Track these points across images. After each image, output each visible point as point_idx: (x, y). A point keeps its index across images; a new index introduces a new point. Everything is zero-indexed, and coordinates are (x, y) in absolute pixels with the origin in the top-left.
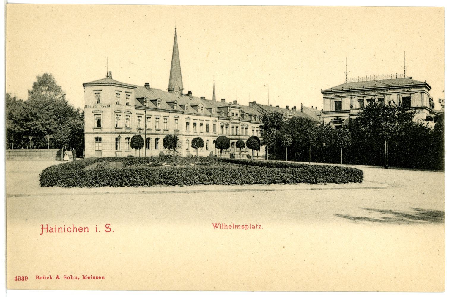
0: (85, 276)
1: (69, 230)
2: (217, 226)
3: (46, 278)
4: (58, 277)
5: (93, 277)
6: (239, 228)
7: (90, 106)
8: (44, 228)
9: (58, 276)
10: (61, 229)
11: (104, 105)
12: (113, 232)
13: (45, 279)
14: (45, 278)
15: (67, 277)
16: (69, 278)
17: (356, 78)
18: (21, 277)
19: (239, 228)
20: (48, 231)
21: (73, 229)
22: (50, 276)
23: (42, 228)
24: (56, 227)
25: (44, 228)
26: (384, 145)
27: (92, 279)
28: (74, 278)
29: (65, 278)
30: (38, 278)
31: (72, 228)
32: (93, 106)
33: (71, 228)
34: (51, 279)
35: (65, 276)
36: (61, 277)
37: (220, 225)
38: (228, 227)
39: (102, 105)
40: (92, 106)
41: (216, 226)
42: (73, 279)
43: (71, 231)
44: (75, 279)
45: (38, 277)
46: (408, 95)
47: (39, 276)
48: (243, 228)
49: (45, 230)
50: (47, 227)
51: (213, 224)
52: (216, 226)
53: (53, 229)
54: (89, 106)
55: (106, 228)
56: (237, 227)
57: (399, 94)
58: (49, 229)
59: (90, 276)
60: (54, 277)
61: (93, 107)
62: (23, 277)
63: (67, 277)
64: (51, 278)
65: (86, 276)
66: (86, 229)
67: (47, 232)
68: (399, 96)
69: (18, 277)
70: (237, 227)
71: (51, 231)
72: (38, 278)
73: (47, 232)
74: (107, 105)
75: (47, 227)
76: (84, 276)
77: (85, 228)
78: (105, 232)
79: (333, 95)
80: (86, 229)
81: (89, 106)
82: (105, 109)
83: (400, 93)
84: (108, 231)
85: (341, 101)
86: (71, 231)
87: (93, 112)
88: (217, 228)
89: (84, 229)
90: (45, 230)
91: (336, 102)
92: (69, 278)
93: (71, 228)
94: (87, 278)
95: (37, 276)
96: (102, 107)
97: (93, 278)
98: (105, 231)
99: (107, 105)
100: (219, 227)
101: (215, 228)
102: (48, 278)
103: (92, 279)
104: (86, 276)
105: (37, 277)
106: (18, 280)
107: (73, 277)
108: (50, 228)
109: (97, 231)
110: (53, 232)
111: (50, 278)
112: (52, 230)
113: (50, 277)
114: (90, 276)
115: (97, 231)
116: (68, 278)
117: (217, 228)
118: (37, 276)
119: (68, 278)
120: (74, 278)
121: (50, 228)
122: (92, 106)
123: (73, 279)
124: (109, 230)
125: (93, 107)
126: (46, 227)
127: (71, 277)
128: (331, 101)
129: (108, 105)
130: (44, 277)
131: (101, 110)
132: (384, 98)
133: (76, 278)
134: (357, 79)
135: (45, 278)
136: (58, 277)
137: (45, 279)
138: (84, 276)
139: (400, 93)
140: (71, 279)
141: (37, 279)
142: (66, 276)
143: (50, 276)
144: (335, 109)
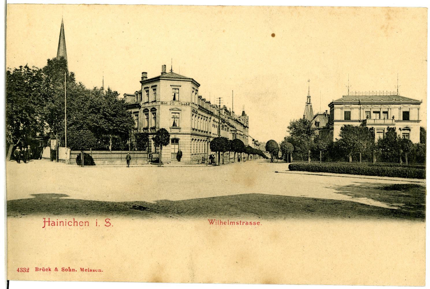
0: (82, 269)
1: (81, 224)
2: (213, 222)
3: (45, 270)
4: (56, 269)
5: (90, 270)
6: (233, 223)
7: (167, 103)
8: (46, 222)
9: (56, 268)
10: (62, 223)
11: (183, 103)
12: (99, 226)
13: (44, 271)
14: (44, 270)
15: (65, 269)
16: (66, 270)
17: (370, 92)
18: (26, 269)
19: (233, 223)
20: (50, 224)
21: (74, 223)
22: (49, 268)
23: (45, 222)
24: (57, 221)
25: (46, 222)
26: (56, 153)
27: (89, 271)
28: (72, 270)
29: (63, 270)
30: (37, 270)
31: (73, 222)
32: (170, 103)
33: (83, 223)
34: (50, 271)
35: (63, 268)
36: (60, 269)
37: (215, 221)
38: (223, 223)
39: (181, 103)
40: (169, 103)
41: (212, 222)
42: (71, 271)
43: (71, 225)
44: (73, 271)
45: (37, 268)
46: (407, 110)
47: (38, 268)
48: (255, 224)
49: (47, 224)
50: (49, 220)
51: (209, 220)
52: (212, 222)
53: (54, 222)
54: (166, 102)
55: (106, 223)
56: (231, 223)
57: (342, 109)
58: (50, 223)
59: (87, 269)
60: (53, 269)
61: (171, 104)
62: (21, 269)
63: (65, 269)
64: (50, 270)
65: (83, 269)
66: (87, 224)
67: (49, 225)
68: (400, 110)
69: (24, 269)
70: (231, 223)
71: (53, 224)
72: (37, 270)
73: (49, 225)
74: (186, 103)
75: (49, 220)
76: (81, 268)
77: (85, 222)
78: (105, 226)
79: (343, 106)
80: (87, 224)
81: (166, 102)
82: (183, 108)
83: (343, 108)
84: (108, 225)
85: (350, 112)
86: (71, 225)
87: (170, 110)
88: (212, 224)
89: (84, 223)
90: (47, 224)
91: (403, 112)
92: (66, 270)
93: (72, 222)
94: (84, 270)
95: (36, 268)
96: (181, 104)
97: (90, 270)
98: (105, 225)
99: (186, 103)
100: (215, 223)
101: (210, 224)
102: (47, 270)
103: (89, 271)
104: (83, 269)
105: (36, 269)
106: (20, 271)
107: (71, 269)
108: (52, 221)
109: (97, 226)
110: (55, 225)
111: (48, 270)
112: (53, 223)
113: (48, 269)
114: (87, 269)
115: (97, 226)
116: (66, 270)
117: (212, 224)
118: (36, 268)
119: (66, 270)
120: (72, 270)
121: (52, 221)
122: (169, 103)
123: (71, 271)
124: (108, 224)
125: (171, 104)
126: (48, 221)
127: (69, 269)
128: (342, 110)
129: (188, 103)
130: (43, 269)
131: (179, 108)
132: (388, 111)
133: (74, 270)
134: (381, 93)
135: (44, 270)
136: (56, 269)
137: (44, 271)
138: (81, 268)
139: (343, 108)
140: (69, 271)
141: (36, 271)
142: (64, 268)
143: (49, 268)
144: (345, 119)
